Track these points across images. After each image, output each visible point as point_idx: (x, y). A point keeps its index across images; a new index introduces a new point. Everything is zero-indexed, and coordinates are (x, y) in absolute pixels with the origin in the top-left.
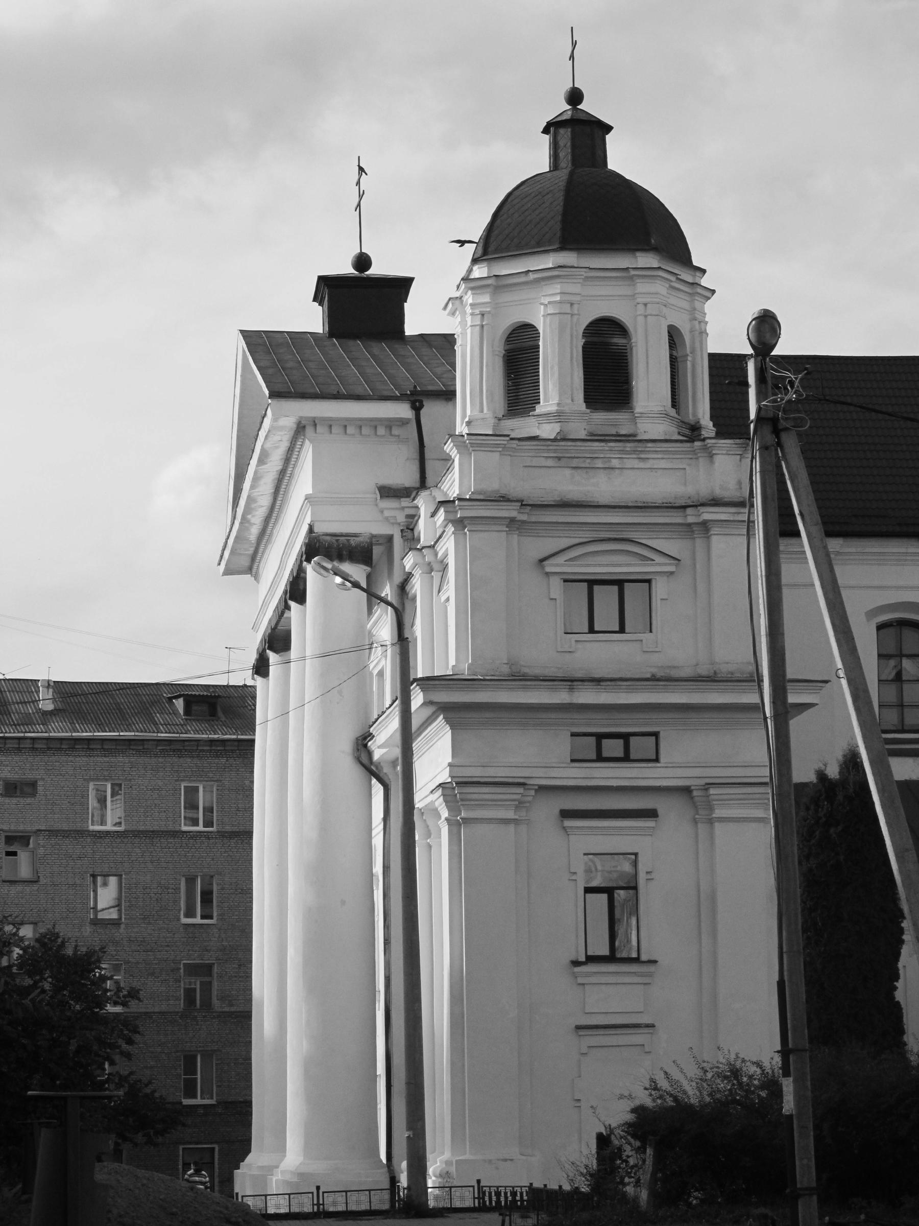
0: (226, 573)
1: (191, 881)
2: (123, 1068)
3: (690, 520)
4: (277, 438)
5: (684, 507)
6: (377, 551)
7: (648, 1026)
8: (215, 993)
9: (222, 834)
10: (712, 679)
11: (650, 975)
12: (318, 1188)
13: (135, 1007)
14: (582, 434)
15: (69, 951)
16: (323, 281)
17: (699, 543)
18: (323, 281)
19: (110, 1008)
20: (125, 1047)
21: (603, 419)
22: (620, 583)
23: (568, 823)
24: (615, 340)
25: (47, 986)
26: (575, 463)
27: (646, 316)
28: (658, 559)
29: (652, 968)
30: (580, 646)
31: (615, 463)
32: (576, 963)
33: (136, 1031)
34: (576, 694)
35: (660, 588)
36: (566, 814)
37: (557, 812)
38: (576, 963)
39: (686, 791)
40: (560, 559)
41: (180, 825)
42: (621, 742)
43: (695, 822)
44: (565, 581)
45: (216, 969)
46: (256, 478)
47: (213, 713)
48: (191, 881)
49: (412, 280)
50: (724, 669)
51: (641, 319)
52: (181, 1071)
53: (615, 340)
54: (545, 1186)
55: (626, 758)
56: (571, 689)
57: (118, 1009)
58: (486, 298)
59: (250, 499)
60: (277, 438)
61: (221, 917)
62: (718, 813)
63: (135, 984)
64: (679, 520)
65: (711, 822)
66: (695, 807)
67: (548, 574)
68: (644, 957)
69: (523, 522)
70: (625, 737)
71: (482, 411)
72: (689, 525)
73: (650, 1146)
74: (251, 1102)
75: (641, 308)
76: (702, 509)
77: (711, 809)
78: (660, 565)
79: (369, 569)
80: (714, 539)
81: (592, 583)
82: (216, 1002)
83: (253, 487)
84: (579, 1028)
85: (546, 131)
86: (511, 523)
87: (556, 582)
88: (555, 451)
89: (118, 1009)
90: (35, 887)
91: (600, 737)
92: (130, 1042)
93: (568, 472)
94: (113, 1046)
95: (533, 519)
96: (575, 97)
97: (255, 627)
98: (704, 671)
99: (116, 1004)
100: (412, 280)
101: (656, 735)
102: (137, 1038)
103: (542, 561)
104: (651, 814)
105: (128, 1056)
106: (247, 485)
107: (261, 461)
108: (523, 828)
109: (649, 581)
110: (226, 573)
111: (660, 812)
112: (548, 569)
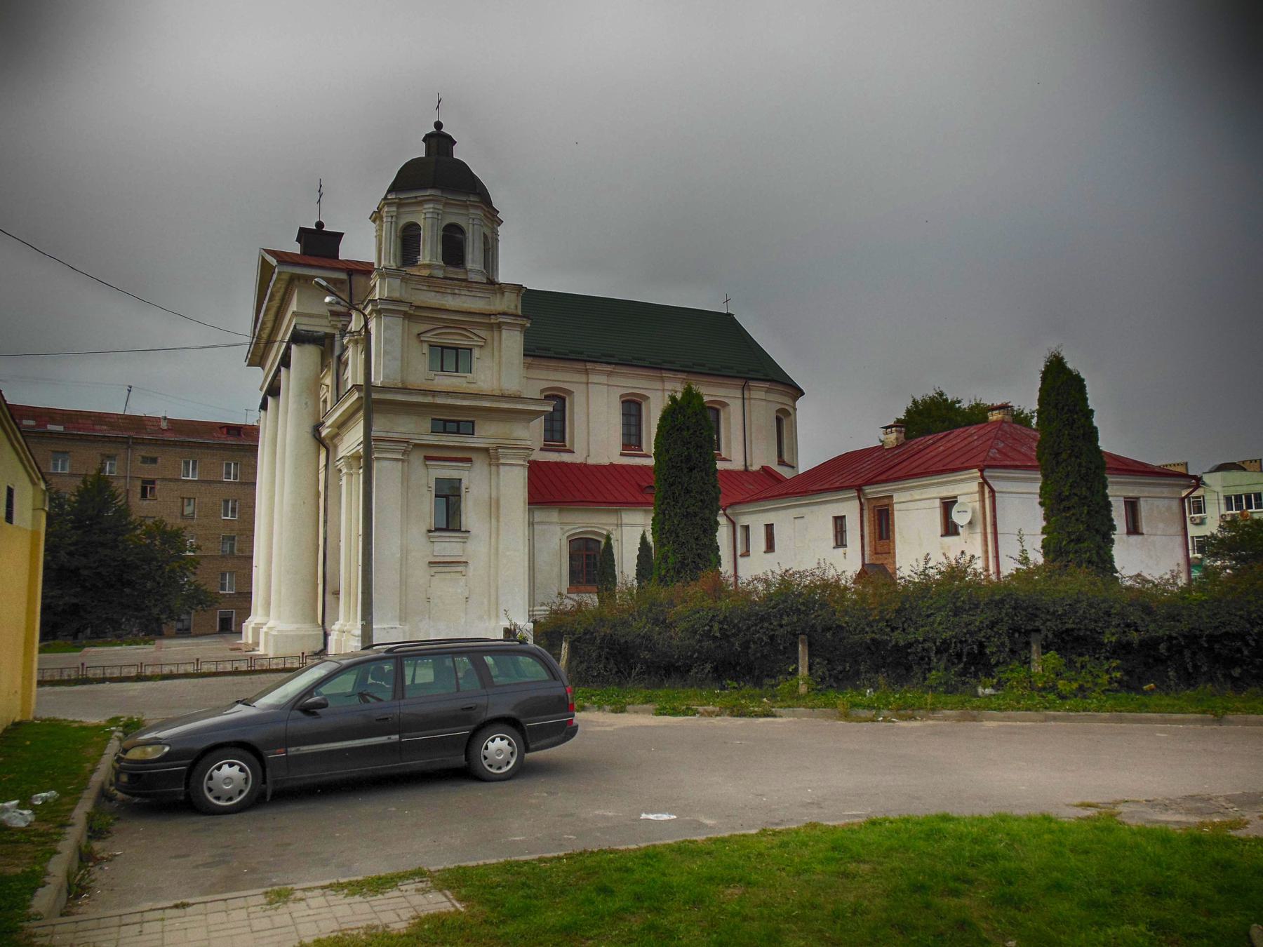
0: (248, 365)
1: (226, 502)
2: (193, 579)
3: (492, 321)
4: (279, 286)
5: (490, 315)
6: (327, 341)
7: (464, 562)
8: (236, 548)
9: (241, 483)
10: (503, 397)
11: (467, 538)
12: (303, 653)
13: (199, 553)
14: (441, 276)
15: (168, 528)
16: (302, 230)
17: (496, 334)
18: (302, 230)
19: (188, 553)
20: (193, 570)
21: (453, 272)
22: (457, 349)
23: (428, 463)
24: (458, 235)
25: (157, 543)
26: (437, 289)
27: (473, 225)
28: (476, 339)
29: (467, 535)
30: (437, 377)
31: (456, 291)
32: (430, 531)
33: (198, 563)
34: (436, 398)
35: (476, 353)
36: (427, 458)
37: (422, 457)
38: (430, 531)
39: (486, 450)
40: (429, 335)
41: (221, 476)
42: (456, 424)
43: (490, 465)
44: (430, 346)
45: (236, 538)
46: (267, 310)
47: (239, 435)
48: (226, 502)
49: (341, 235)
50: (507, 393)
51: (471, 226)
52: (219, 579)
53: (458, 235)
54: (900, 815)
55: (458, 432)
56: (434, 396)
57: (192, 554)
58: (394, 209)
59: (263, 323)
60: (279, 286)
61: (240, 517)
62: (502, 461)
63: (200, 543)
64: (487, 321)
65: (498, 465)
66: (491, 458)
67: (422, 341)
68: (463, 529)
69: (411, 315)
70: (458, 422)
71: (390, 262)
72: (492, 324)
73: (565, 641)
74: (251, 593)
75: (471, 221)
76: (499, 316)
77: (498, 459)
78: (477, 341)
79: (322, 348)
80: (504, 331)
81: (443, 348)
82: (236, 551)
83: (265, 315)
84: (430, 563)
85: (424, 140)
86: (406, 316)
87: (426, 349)
88: (428, 282)
89: (192, 554)
90: (155, 502)
91: (446, 421)
92: (196, 568)
93: (433, 294)
94: (188, 569)
95: (416, 313)
96: (438, 125)
97: (261, 389)
98: (497, 392)
99: (190, 551)
100: (341, 235)
101: (473, 422)
102: (198, 566)
103: (419, 334)
104: (469, 460)
105: (194, 574)
106: (262, 315)
107: (270, 300)
108: (406, 464)
109: (471, 350)
110: (248, 365)
111: (473, 459)
112: (422, 339)
